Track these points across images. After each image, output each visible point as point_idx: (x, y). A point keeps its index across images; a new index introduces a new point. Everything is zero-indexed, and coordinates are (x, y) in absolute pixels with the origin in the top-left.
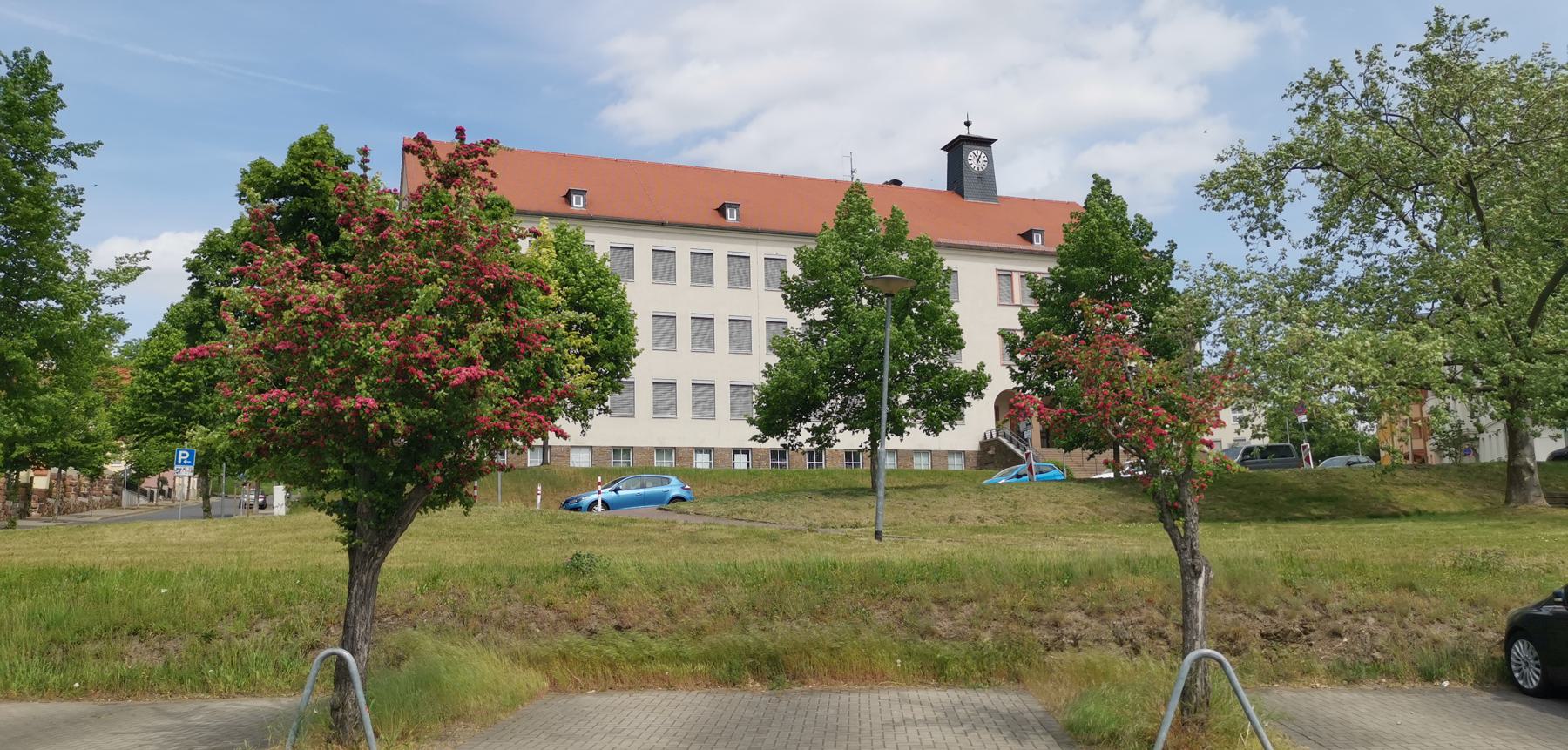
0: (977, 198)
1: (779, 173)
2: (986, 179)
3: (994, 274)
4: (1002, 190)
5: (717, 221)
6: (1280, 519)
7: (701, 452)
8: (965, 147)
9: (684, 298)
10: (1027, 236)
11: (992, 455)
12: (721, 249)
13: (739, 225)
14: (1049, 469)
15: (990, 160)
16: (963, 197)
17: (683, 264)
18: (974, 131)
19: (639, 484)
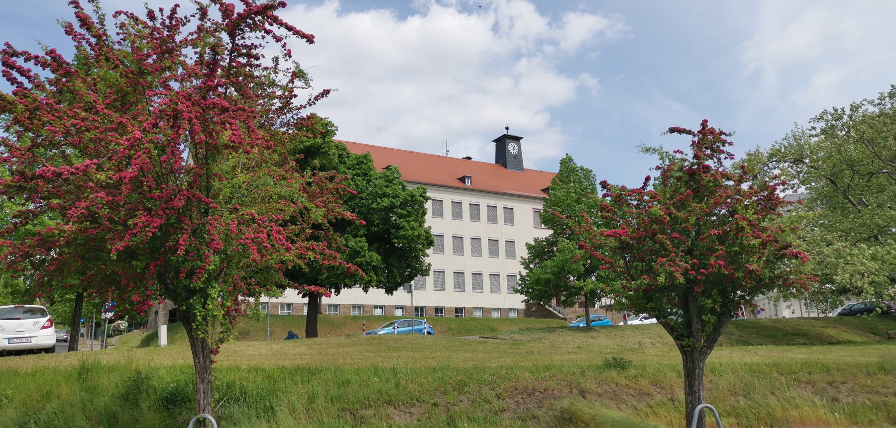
0: (513, 169)
1: (410, 150)
2: (518, 158)
3: (532, 211)
4: (527, 164)
5: (460, 185)
6: (788, 344)
7: (377, 308)
8: (507, 141)
9: (467, 228)
10: (462, 179)
11: (534, 311)
12: (466, 200)
13: (471, 187)
14: (604, 318)
15: (520, 149)
16: (506, 168)
17: (466, 210)
18: (511, 133)
19: (406, 325)
